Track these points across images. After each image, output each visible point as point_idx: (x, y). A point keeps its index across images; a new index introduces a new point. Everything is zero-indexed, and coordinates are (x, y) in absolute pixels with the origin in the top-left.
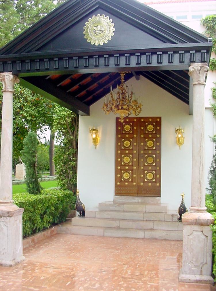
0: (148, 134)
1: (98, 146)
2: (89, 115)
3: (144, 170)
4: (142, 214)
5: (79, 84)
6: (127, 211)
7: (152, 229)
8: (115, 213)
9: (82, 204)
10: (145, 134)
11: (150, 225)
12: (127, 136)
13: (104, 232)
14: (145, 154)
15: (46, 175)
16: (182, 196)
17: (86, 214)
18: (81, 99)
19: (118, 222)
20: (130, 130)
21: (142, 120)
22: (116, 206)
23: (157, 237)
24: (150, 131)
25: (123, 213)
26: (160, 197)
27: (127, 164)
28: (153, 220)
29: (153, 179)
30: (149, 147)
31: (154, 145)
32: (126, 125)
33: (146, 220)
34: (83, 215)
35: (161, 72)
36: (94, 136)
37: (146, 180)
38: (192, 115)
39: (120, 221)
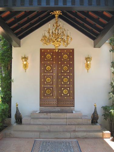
0: (64, 61)
1: (27, 70)
2: (20, 46)
3: (61, 88)
4: (65, 120)
5: (18, 23)
6: (53, 118)
7: (75, 131)
8: (45, 120)
9: (20, 114)
10: (61, 61)
11: (73, 128)
12: (49, 63)
13: (40, 134)
14: (62, 76)
15: (56, 110)
16: (95, 106)
17: (23, 120)
18: (17, 34)
19: (49, 127)
20: (50, 58)
21: (49, 51)
22: (44, 115)
23: (80, 136)
24: (65, 59)
25: (50, 120)
26: (74, 106)
27: (49, 83)
28: (73, 124)
29: (68, 94)
30: (64, 71)
31: (68, 69)
32: (48, 54)
33: (69, 124)
34: (20, 123)
35: (80, 14)
36: (25, 63)
37: (62, 95)
38: (95, 47)
39: (50, 126)
